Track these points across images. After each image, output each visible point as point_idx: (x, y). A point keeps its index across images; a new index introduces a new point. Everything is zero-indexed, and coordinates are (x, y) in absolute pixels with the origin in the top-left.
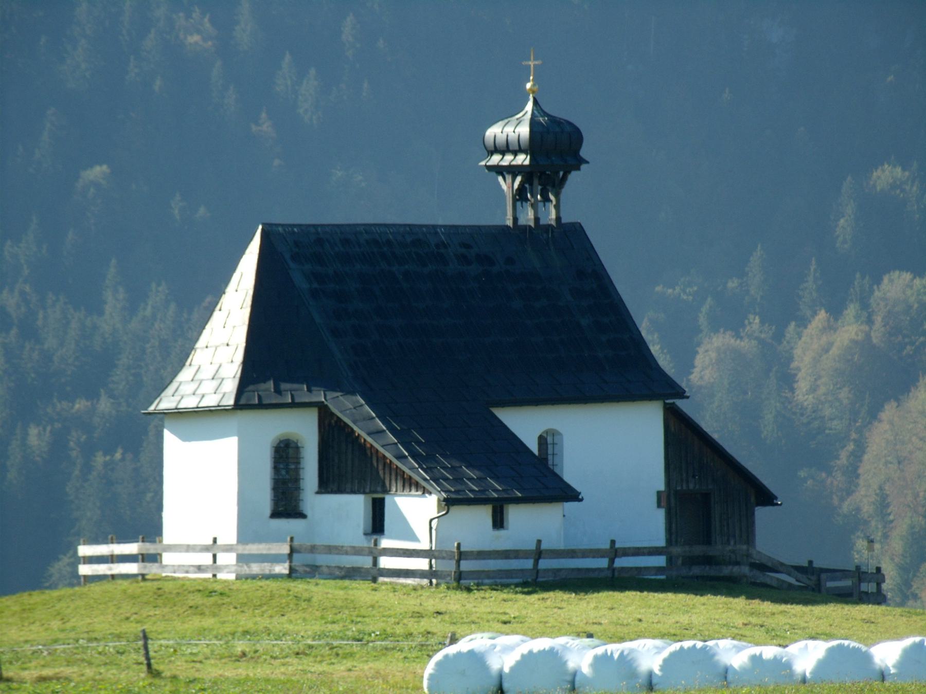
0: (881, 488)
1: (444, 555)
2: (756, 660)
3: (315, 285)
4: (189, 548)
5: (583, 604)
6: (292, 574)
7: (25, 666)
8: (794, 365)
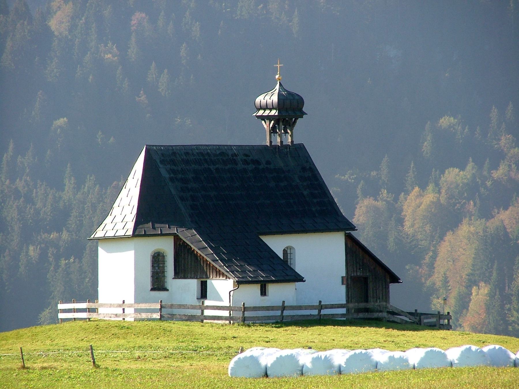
0: (445, 274)
1: (237, 309)
2: (391, 358)
3: (172, 175)
4: (111, 306)
5: (306, 332)
6: (162, 318)
7: (35, 362)
8: (403, 214)
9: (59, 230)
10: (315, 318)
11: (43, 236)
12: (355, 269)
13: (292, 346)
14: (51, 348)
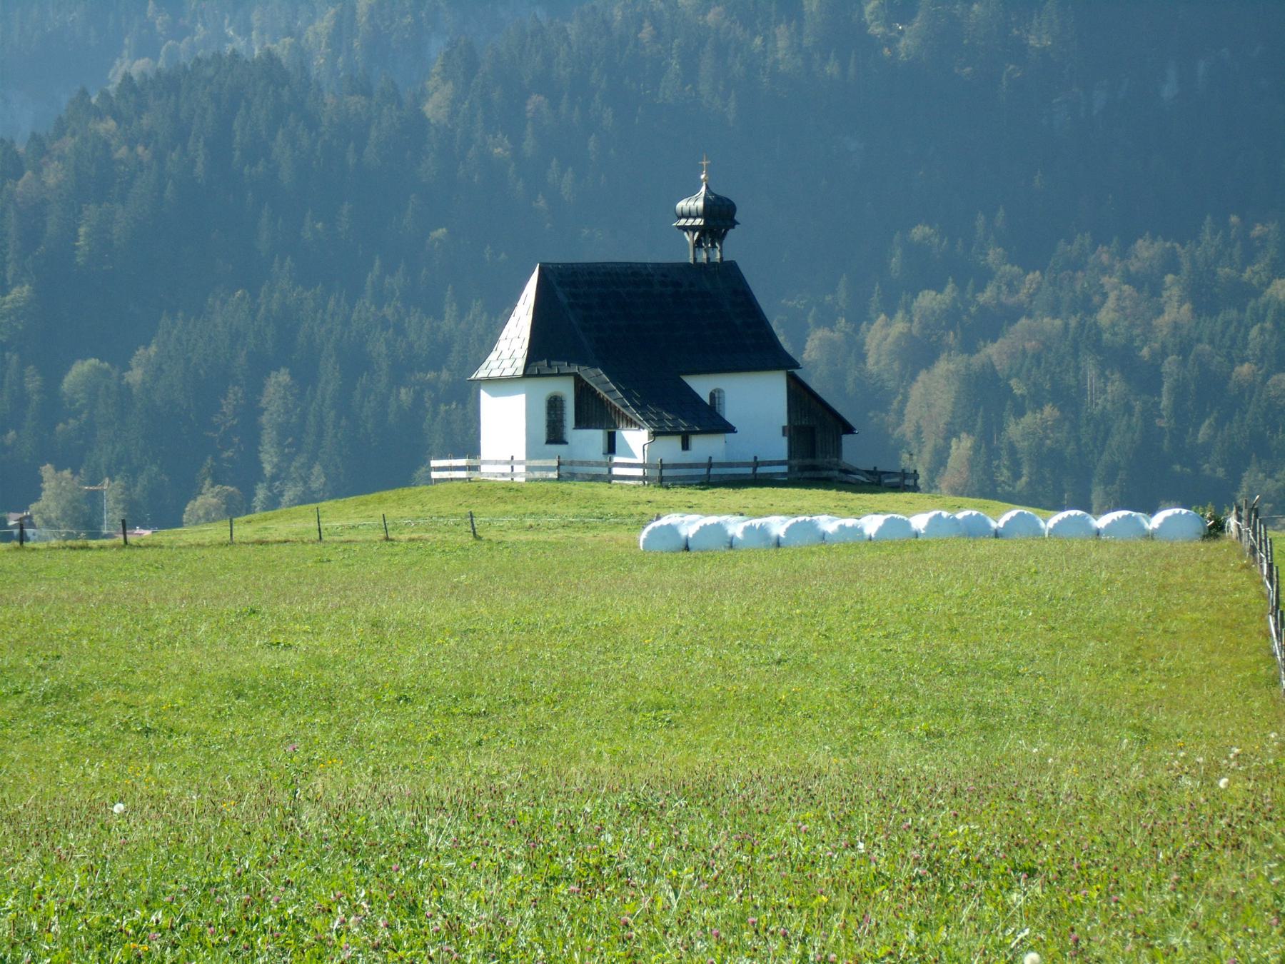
2: (842, 527)
4: (497, 462)
6: (560, 478)
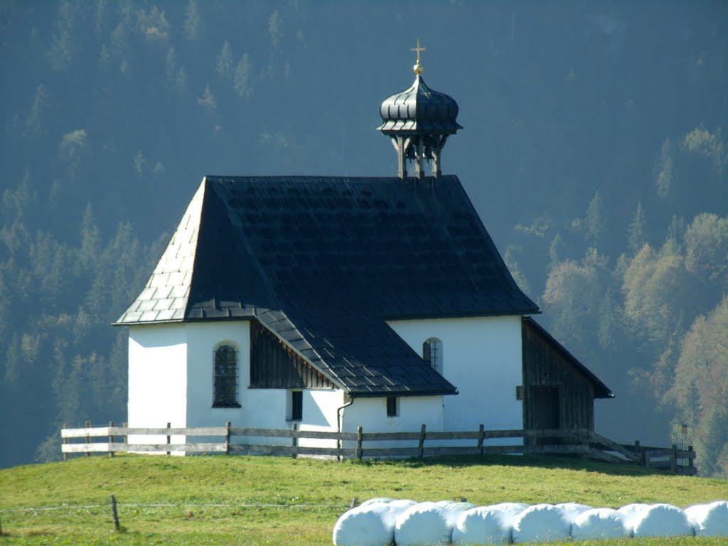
0: (693, 384)
2: (594, 519)
3: (248, 224)
4: (149, 431)
5: (459, 474)
6: (230, 452)
8: (624, 287)
9: (73, 311)
10: (473, 452)
11: (46, 320)
12: (538, 376)
13: (428, 496)
14: (49, 500)
